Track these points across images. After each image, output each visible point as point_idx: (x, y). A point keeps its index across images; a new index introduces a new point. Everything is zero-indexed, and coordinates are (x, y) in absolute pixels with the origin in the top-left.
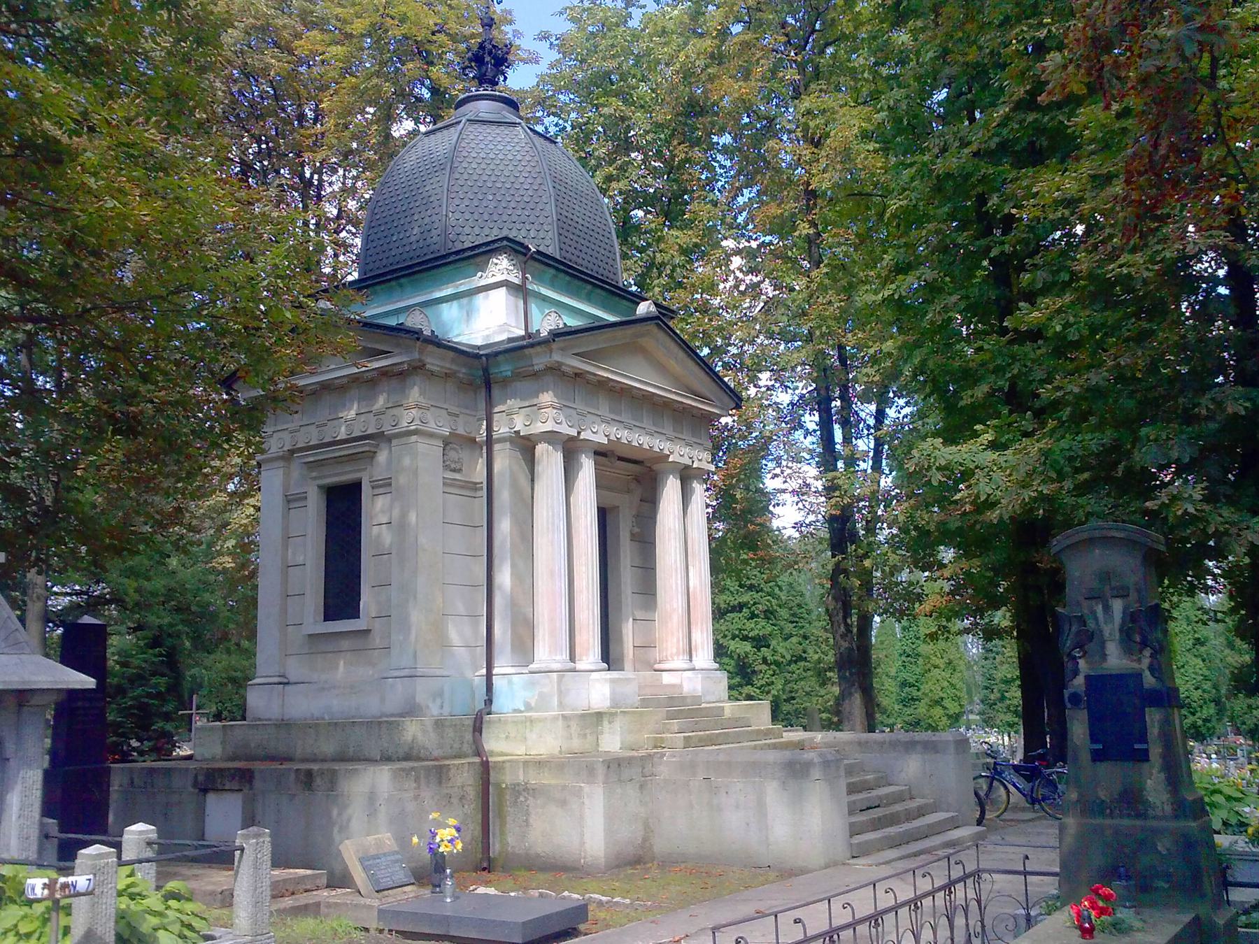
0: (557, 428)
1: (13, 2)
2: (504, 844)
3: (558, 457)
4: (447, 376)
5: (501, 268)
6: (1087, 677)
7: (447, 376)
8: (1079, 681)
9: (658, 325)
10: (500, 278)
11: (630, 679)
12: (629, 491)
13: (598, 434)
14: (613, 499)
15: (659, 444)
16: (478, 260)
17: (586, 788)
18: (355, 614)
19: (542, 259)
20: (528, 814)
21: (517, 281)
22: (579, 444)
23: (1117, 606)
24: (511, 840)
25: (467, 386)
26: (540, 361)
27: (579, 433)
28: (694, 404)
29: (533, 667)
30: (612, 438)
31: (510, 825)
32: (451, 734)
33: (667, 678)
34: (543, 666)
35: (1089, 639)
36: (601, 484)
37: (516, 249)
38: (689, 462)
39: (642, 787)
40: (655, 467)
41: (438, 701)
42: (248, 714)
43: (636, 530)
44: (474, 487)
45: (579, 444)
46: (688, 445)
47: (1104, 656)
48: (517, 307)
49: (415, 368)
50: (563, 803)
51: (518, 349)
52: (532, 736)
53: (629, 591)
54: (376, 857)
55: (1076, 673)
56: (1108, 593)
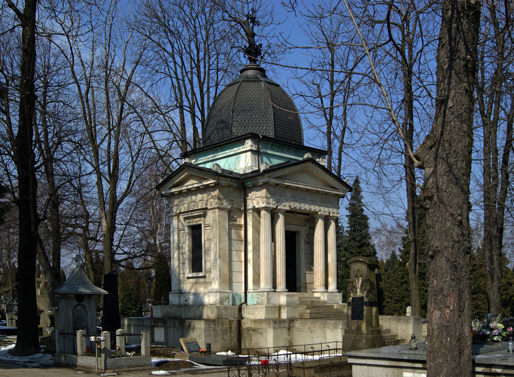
0: (268, 206)
1: (88, 0)
2: (245, 346)
3: (268, 216)
4: (230, 186)
5: (249, 144)
6: (353, 298)
7: (230, 186)
8: (351, 299)
9: (312, 162)
10: (249, 148)
11: (296, 296)
12: (305, 225)
13: (286, 206)
14: (293, 228)
15: (314, 208)
16: (242, 141)
17: (268, 330)
18: (201, 271)
19: (266, 139)
20: (251, 337)
21: (255, 149)
22: (278, 210)
23: (360, 279)
24: (247, 345)
25: (238, 189)
26: (261, 181)
27: (277, 207)
28: (329, 191)
29: (260, 290)
30: (292, 207)
31: (247, 340)
32: (230, 311)
33: (316, 295)
34: (262, 290)
35: (354, 287)
36: (286, 223)
37: (254, 137)
38: (328, 214)
39: (289, 329)
40: (314, 216)
41: (227, 301)
42: (170, 303)
43: (307, 240)
44: (240, 226)
45: (278, 210)
46: (327, 207)
47: (356, 292)
48: (255, 159)
49: (217, 185)
50: (261, 334)
51: (256, 174)
52: (256, 313)
53: (304, 263)
54: (190, 343)
55: (350, 297)
56: (359, 275)
